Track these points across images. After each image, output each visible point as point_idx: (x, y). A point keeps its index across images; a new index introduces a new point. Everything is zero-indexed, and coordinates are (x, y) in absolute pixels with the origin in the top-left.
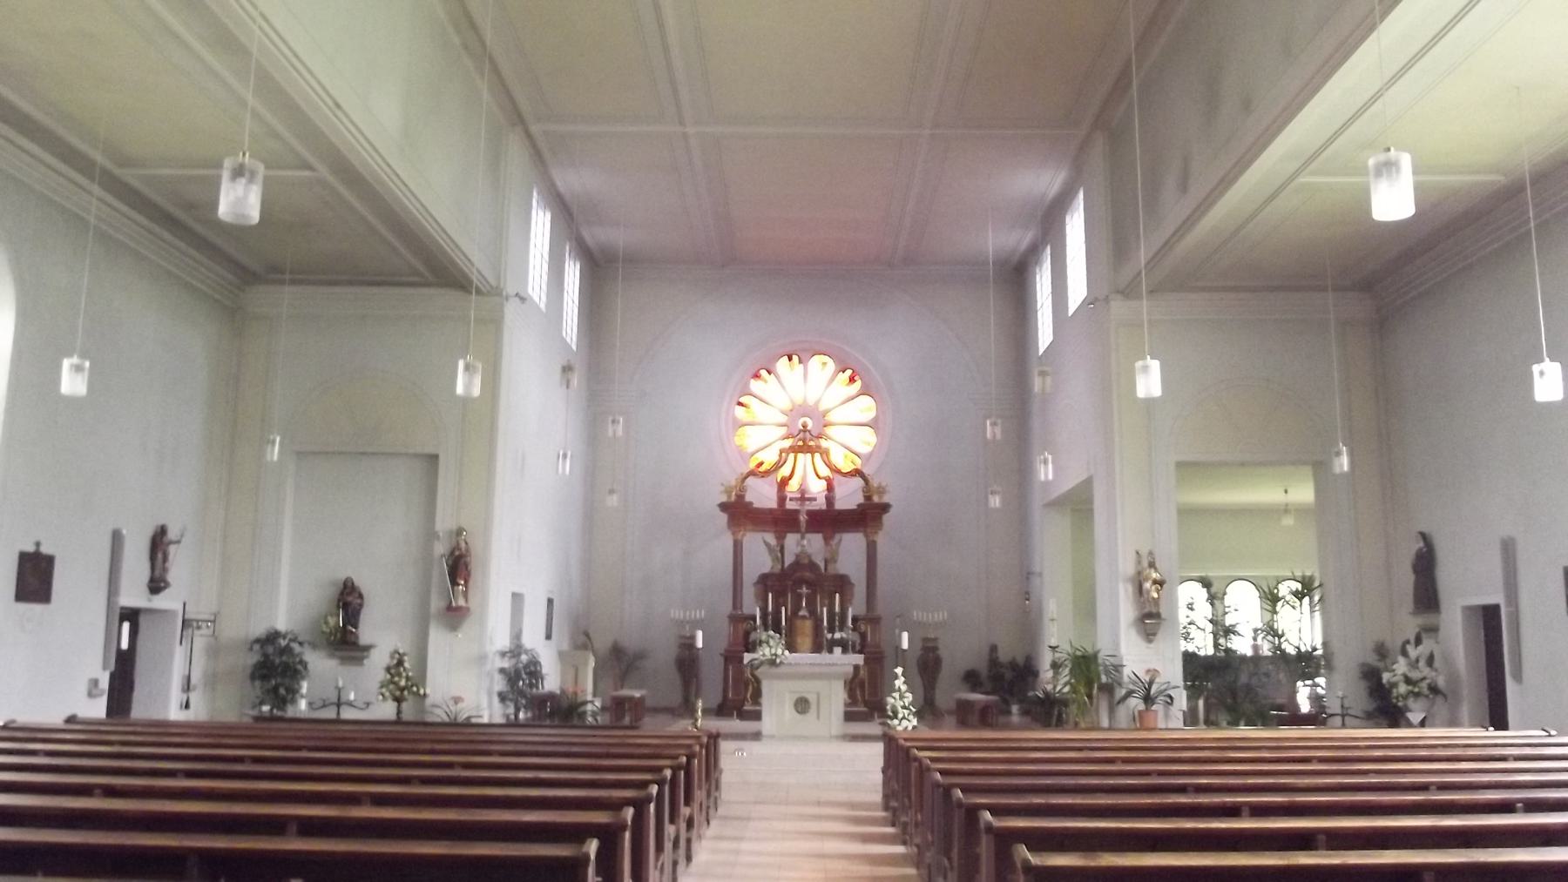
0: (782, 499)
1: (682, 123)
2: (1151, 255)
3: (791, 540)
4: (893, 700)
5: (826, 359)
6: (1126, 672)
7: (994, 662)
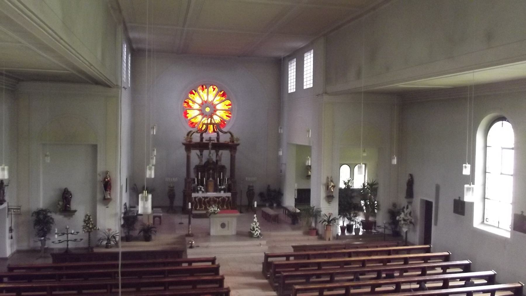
3: (206, 152)
4: (253, 225)
6: (322, 213)
7: (269, 190)
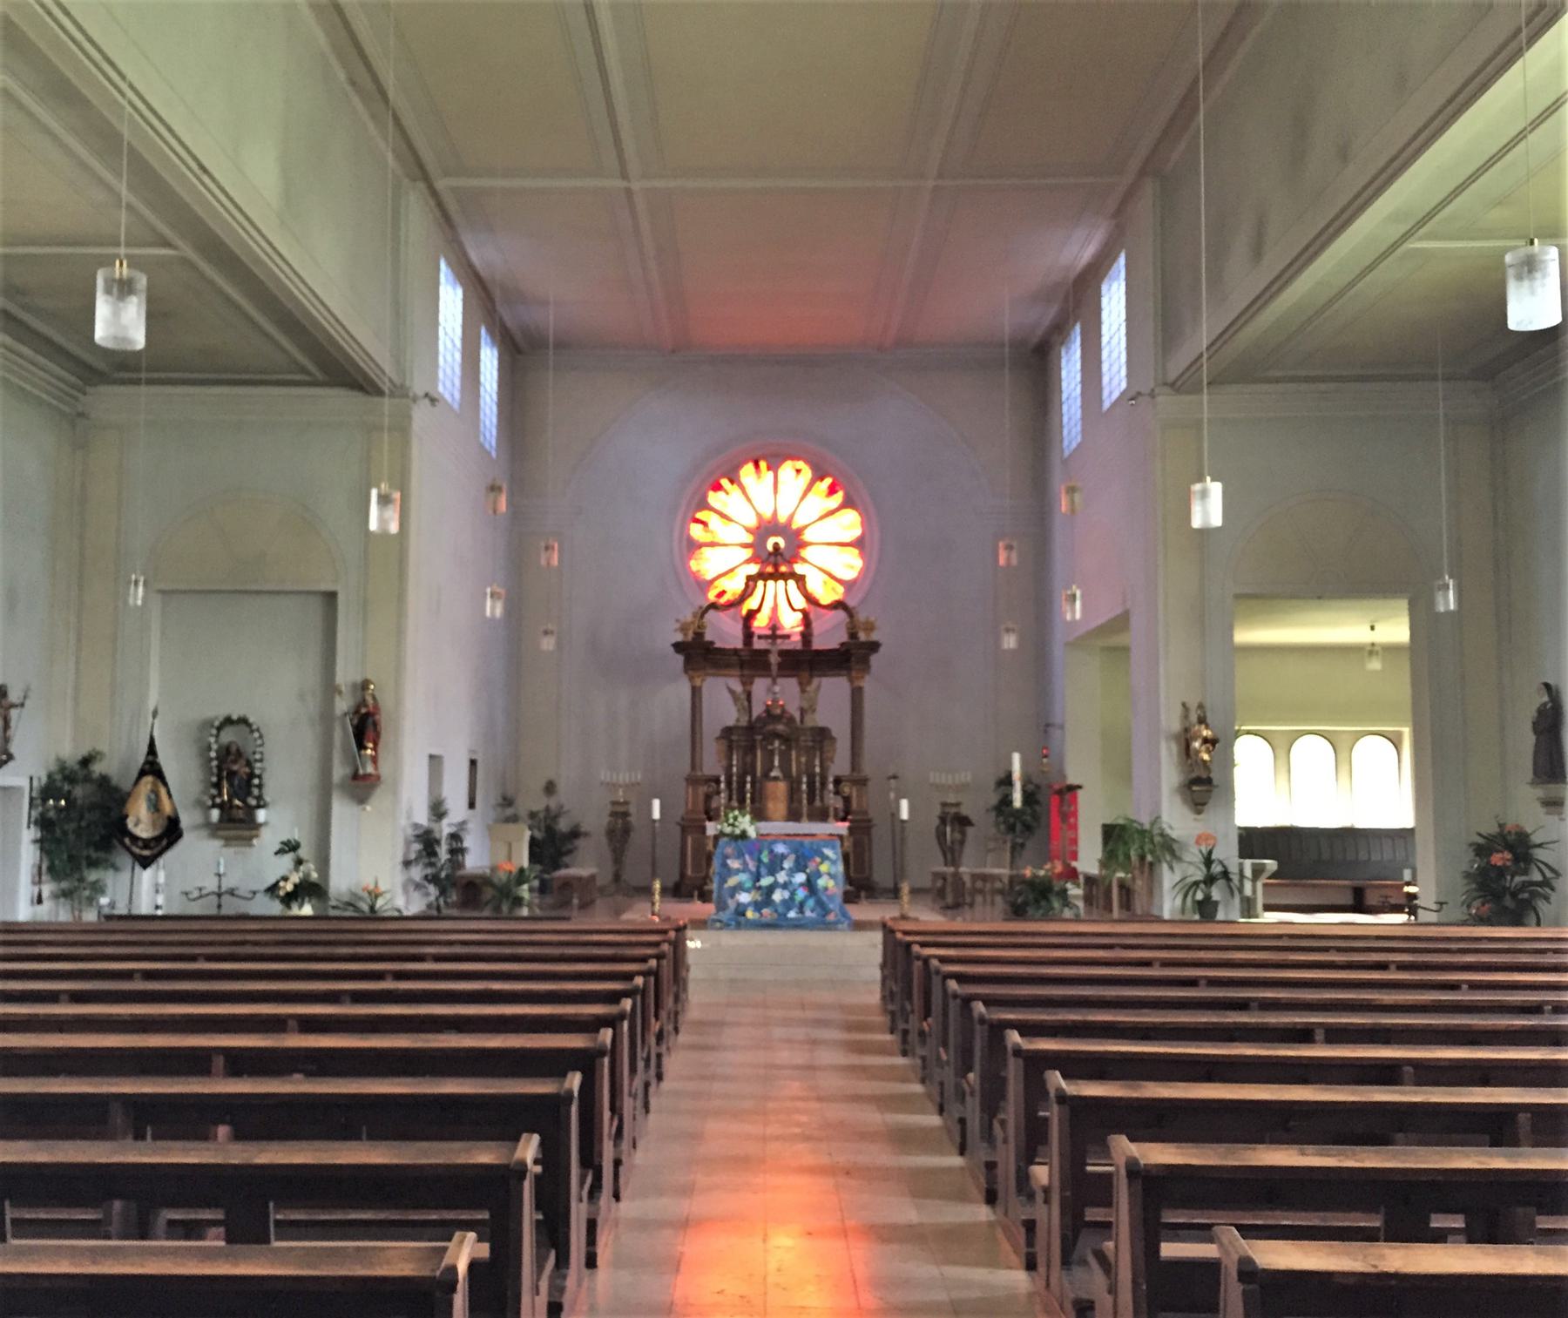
0: (748, 635)
1: (624, 176)
2: (1209, 343)
3: (760, 686)
5: (800, 464)
